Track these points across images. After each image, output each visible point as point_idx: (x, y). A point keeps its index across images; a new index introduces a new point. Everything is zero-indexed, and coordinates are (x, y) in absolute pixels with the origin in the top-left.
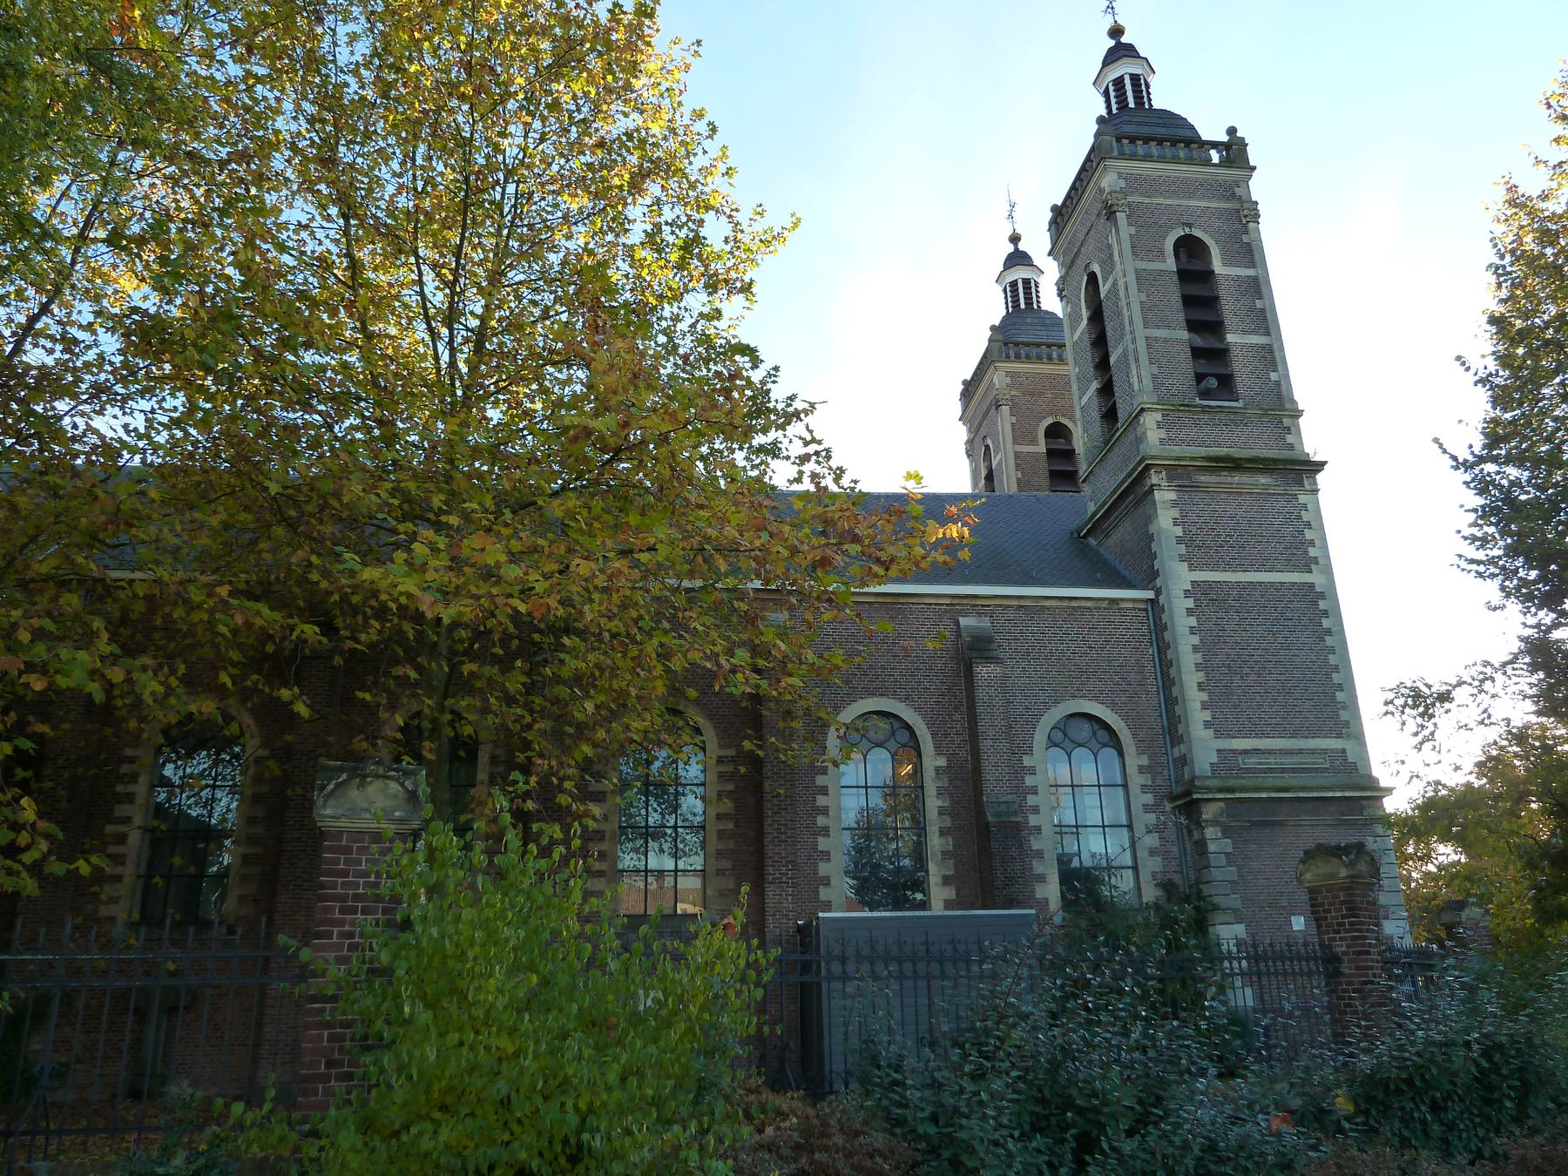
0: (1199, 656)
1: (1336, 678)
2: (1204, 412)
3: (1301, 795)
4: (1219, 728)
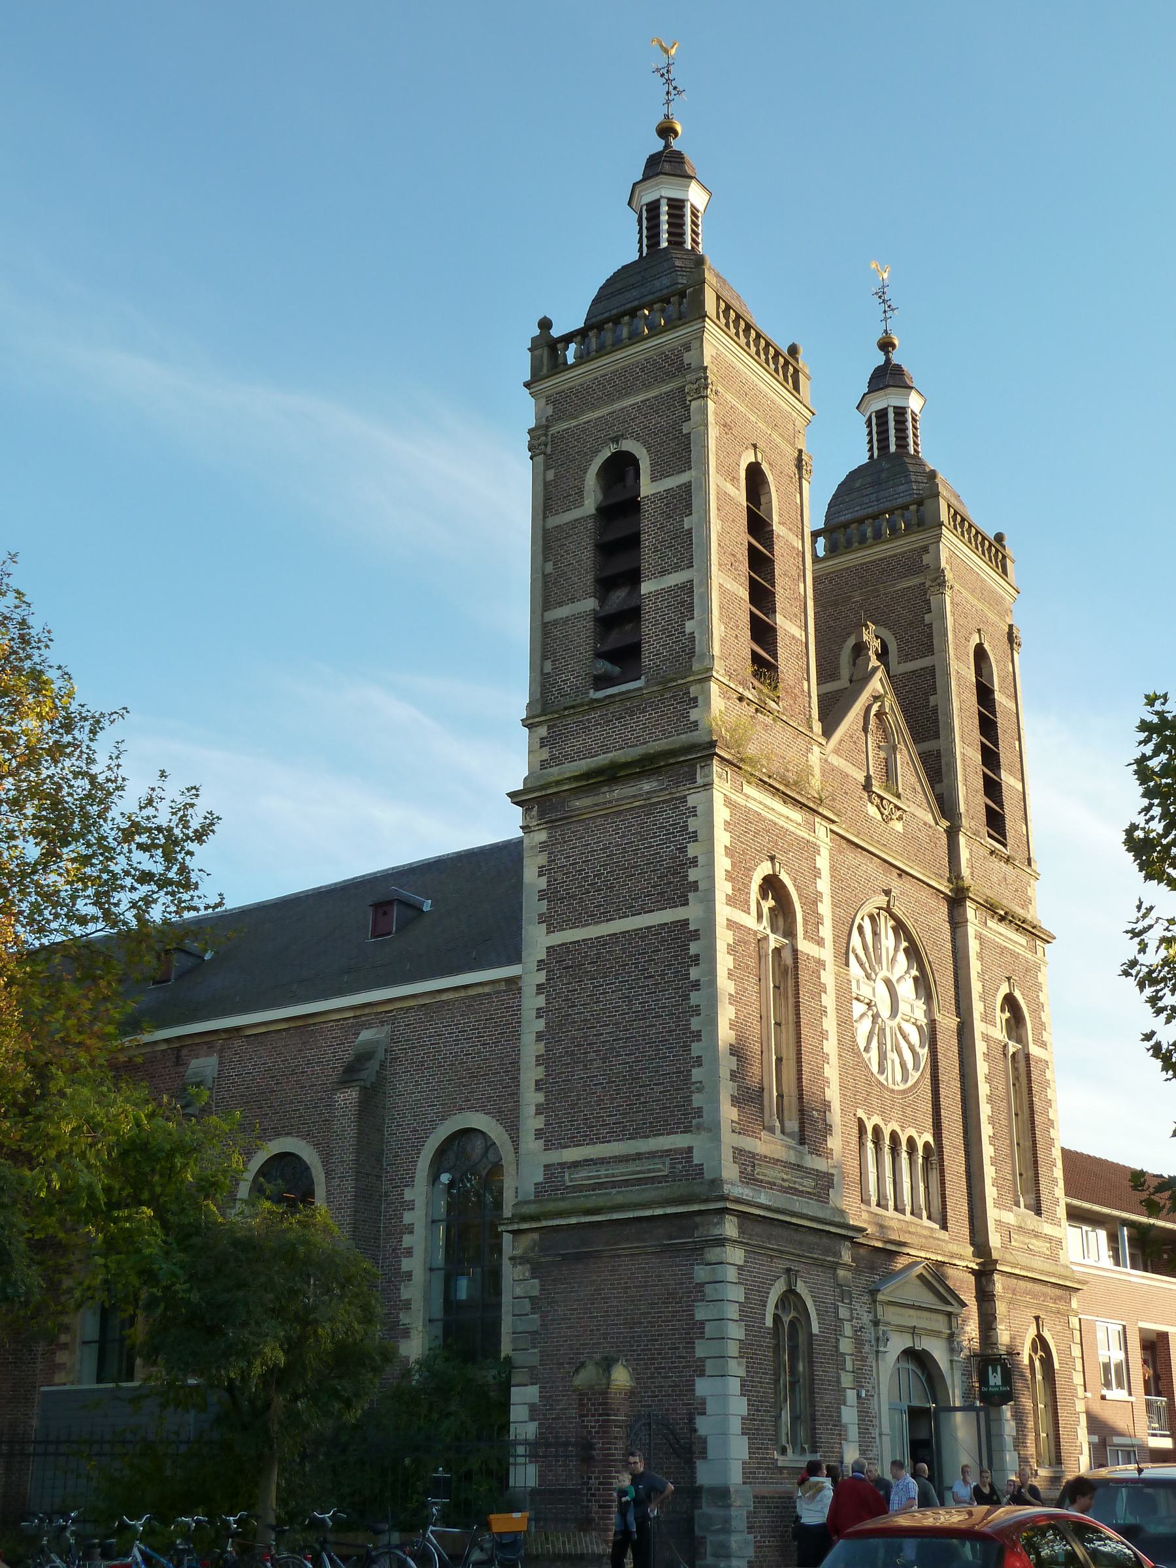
0: (542, 1045)
2: (593, 709)
3: (615, 1216)
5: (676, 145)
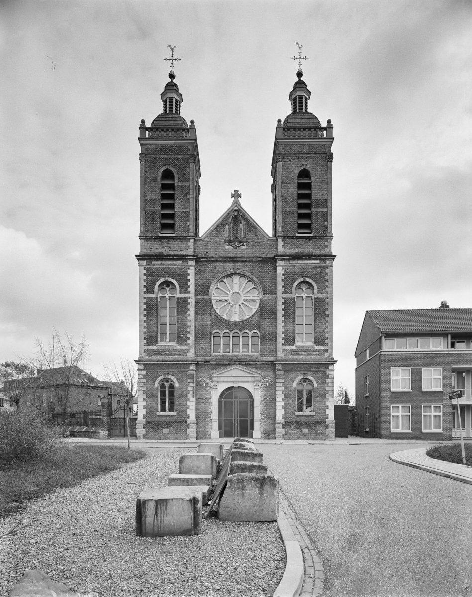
5: (302, 79)
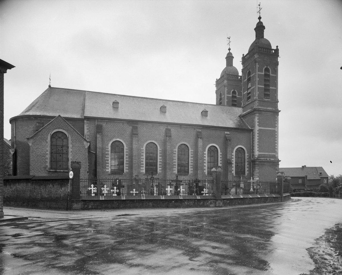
1: (276, 139)
4: (259, 151)
